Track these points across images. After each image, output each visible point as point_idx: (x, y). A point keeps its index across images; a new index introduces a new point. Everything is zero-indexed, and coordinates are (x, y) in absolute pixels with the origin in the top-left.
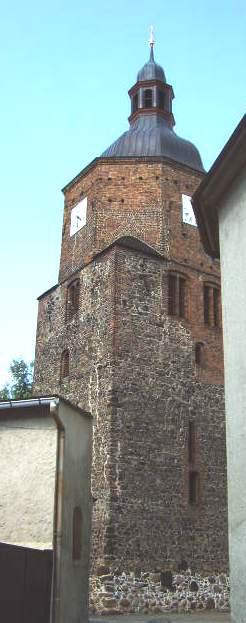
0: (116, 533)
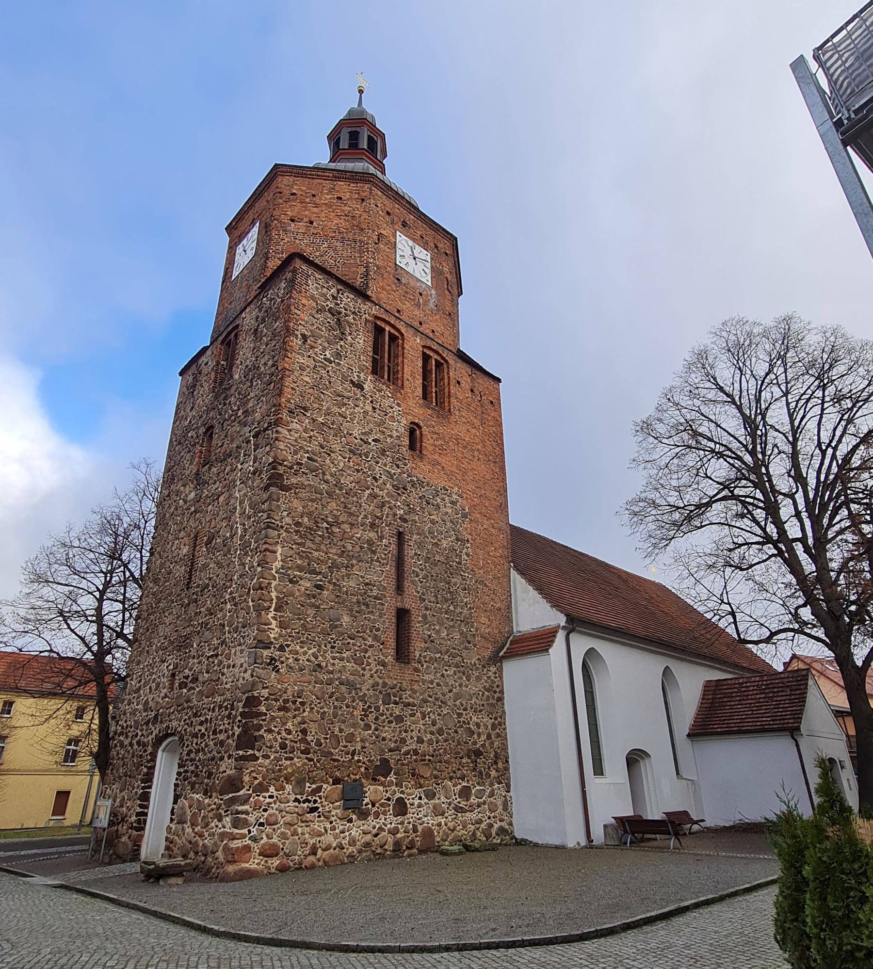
0: (263, 709)
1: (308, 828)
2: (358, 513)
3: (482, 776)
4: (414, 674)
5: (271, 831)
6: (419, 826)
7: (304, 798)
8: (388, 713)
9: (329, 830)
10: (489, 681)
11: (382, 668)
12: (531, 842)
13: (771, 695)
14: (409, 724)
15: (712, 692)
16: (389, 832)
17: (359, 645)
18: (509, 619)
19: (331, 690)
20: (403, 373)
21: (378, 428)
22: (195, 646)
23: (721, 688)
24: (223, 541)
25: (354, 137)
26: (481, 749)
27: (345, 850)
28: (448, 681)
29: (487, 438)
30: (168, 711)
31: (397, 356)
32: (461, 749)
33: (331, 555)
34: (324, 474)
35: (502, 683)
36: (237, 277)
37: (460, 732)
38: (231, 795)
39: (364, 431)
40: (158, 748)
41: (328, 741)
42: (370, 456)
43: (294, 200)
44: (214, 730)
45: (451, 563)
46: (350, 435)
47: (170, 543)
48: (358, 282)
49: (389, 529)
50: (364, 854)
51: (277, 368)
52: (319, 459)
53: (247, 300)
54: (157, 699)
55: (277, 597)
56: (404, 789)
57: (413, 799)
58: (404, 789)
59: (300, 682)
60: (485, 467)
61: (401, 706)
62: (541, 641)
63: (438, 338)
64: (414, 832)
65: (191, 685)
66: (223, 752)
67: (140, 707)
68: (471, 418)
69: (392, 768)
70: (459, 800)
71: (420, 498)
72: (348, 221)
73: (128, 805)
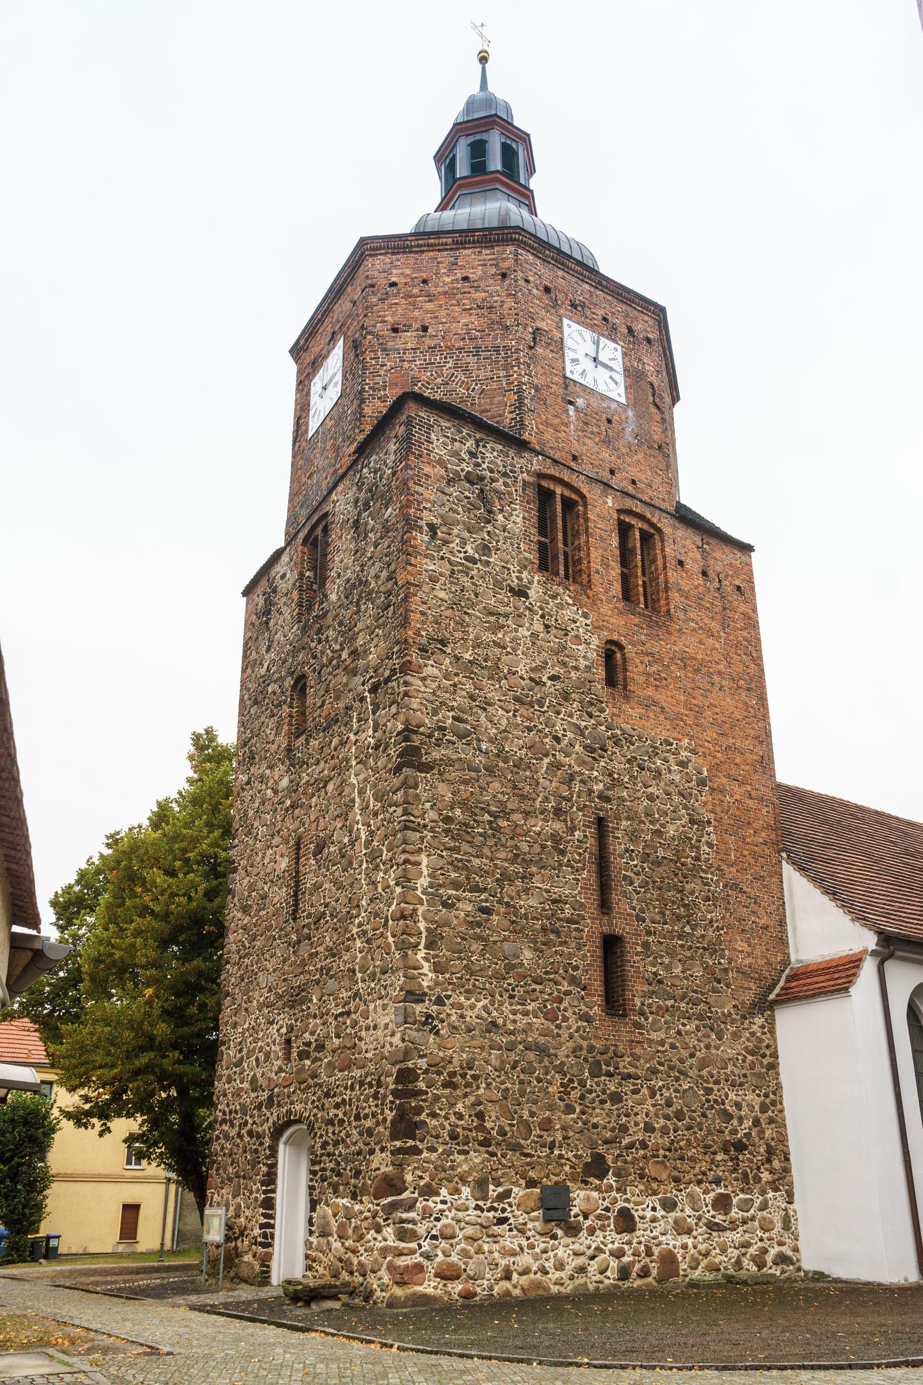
0: (422, 1085)
2: (534, 796)
3: (747, 1181)
5: (448, 1246)
6: (654, 1248)
7: (489, 1205)
8: (598, 1089)
10: (753, 1039)
11: (585, 1024)
14: (631, 1104)
17: (549, 991)
18: (782, 942)
19: (513, 1057)
20: (589, 562)
21: (555, 658)
22: (315, 1001)
24: (340, 850)
25: (478, 150)
26: (744, 1140)
28: (687, 1040)
29: (733, 650)
31: (576, 535)
32: (714, 1141)
33: (498, 862)
35: (775, 1041)
36: (317, 432)
37: (710, 1116)
38: (390, 1199)
39: (534, 665)
40: (278, 1140)
41: (515, 1129)
42: (547, 704)
43: (395, 296)
45: (683, 860)
46: (514, 674)
47: (260, 854)
48: (507, 421)
51: (396, 583)
53: (335, 471)
54: (269, 1074)
55: (428, 930)
58: (629, 1196)
59: (469, 1047)
61: (617, 1079)
62: (837, 976)
63: (642, 492)
65: (316, 1054)
66: (372, 1143)
67: (246, 1085)
68: (706, 620)
69: (609, 1167)
71: (629, 761)
72: (484, 316)
73: (247, 1214)
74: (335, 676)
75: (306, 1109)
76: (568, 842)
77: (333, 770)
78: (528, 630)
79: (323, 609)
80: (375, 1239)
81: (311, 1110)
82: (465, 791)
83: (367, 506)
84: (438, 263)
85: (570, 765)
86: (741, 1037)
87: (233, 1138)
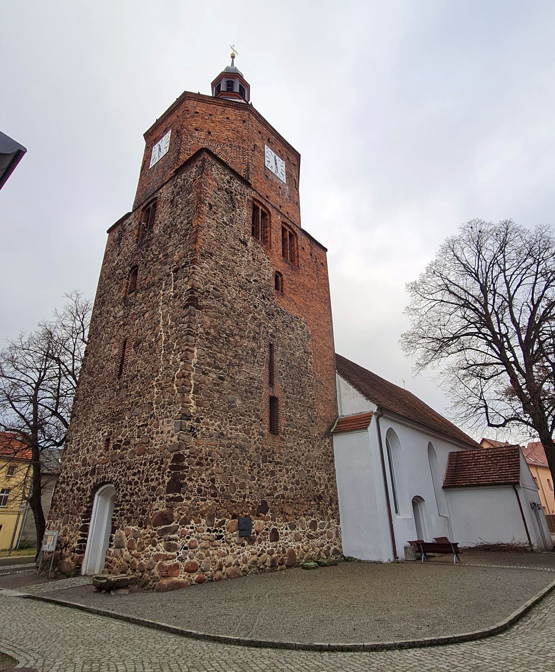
0: (186, 463)
1: (216, 551)
2: (245, 329)
4: (281, 442)
5: (192, 553)
6: (286, 549)
7: (214, 529)
9: (230, 552)
10: (325, 448)
11: (261, 437)
12: (356, 559)
13: (496, 461)
15: (455, 460)
16: (268, 553)
17: (247, 420)
18: (336, 407)
19: (230, 451)
20: (271, 238)
22: (127, 419)
23: (461, 457)
24: (149, 345)
25: (230, 85)
26: (322, 495)
27: (240, 567)
28: (301, 448)
30: (104, 466)
31: (266, 227)
32: (310, 495)
33: (228, 357)
34: (224, 300)
37: (309, 483)
38: (163, 527)
40: (95, 493)
41: (228, 488)
42: (252, 291)
43: (197, 117)
44: (146, 479)
45: (301, 368)
47: (103, 347)
49: (264, 342)
50: (253, 569)
51: (192, 225)
52: (220, 290)
53: (163, 181)
55: (195, 384)
56: (276, 522)
57: (282, 529)
59: (210, 445)
60: (320, 305)
64: (283, 553)
66: (155, 495)
70: (310, 530)
71: (282, 322)
72: (234, 134)
73: (70, 534)
74: (154, 266)
75: (115, 476)
76: (258, 353)
77: (149, 307)
78: (247, 258)
79: (150, 237)
80: (152, 550)
81: (118, 477)
82: (217, 322)
83: (178, 194)
84: (217, 110)
85: (260, 319)
86: (321, 447)
87: (67, 491)
